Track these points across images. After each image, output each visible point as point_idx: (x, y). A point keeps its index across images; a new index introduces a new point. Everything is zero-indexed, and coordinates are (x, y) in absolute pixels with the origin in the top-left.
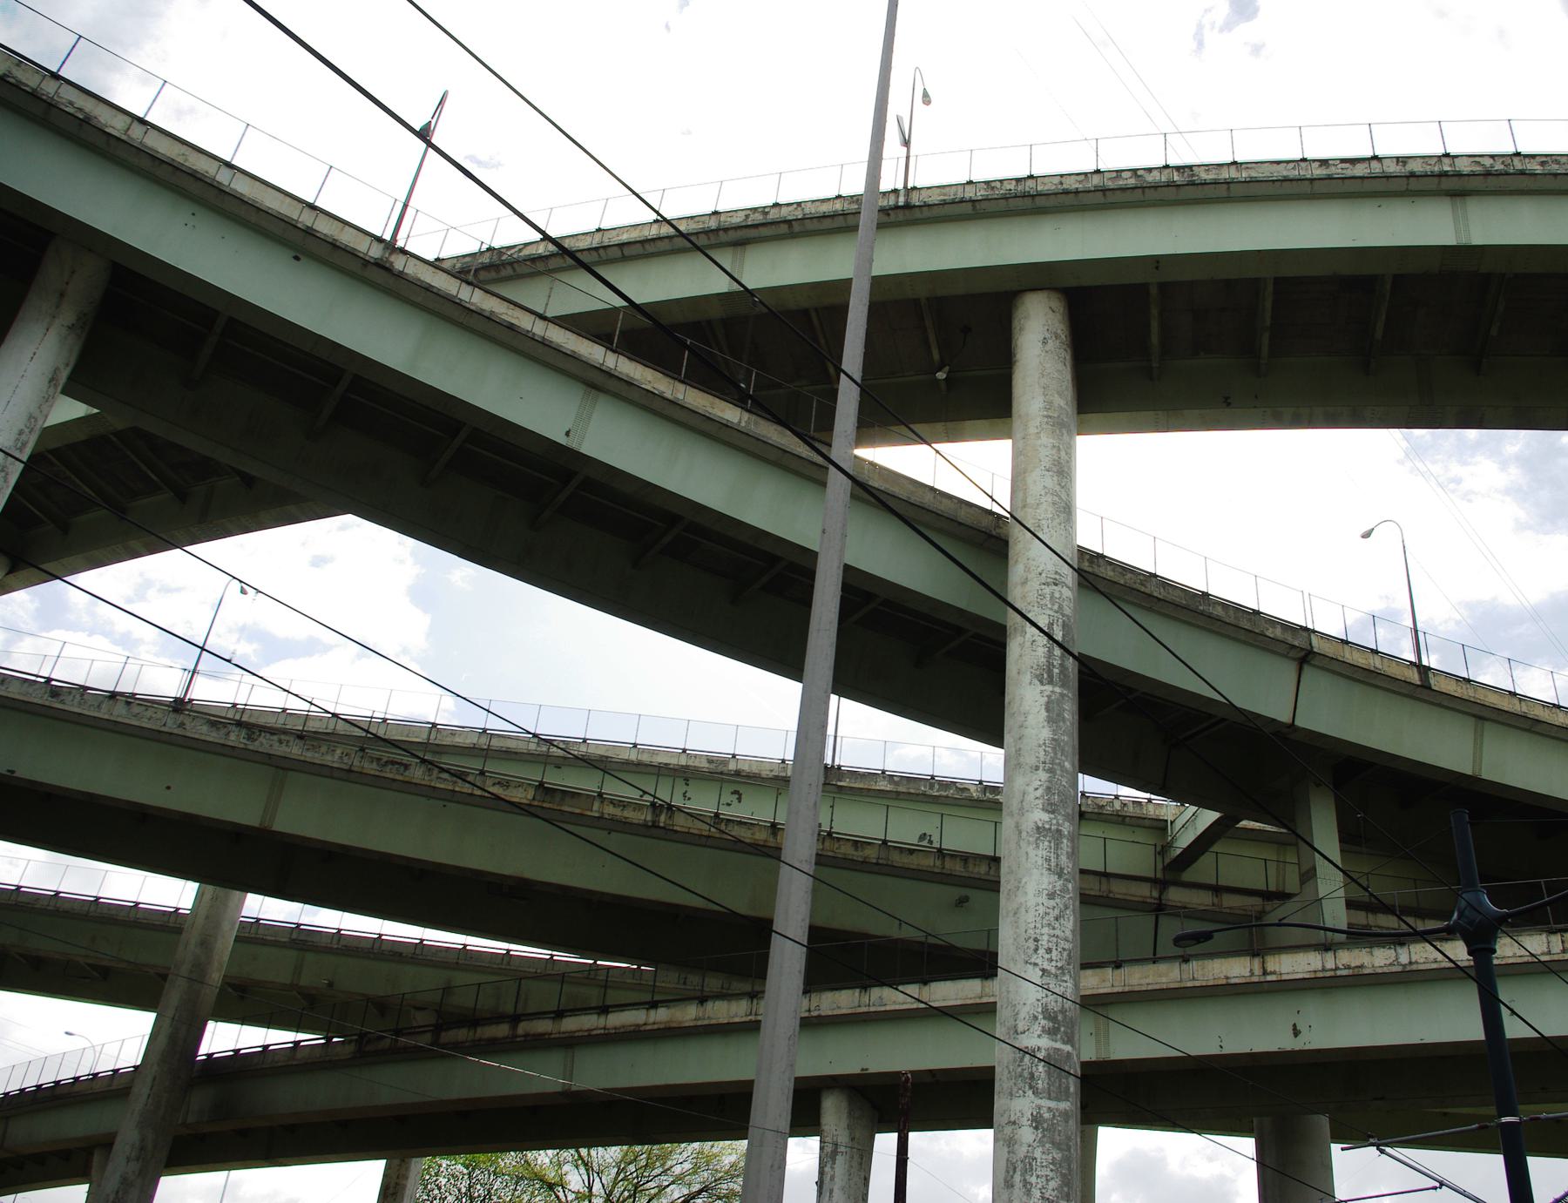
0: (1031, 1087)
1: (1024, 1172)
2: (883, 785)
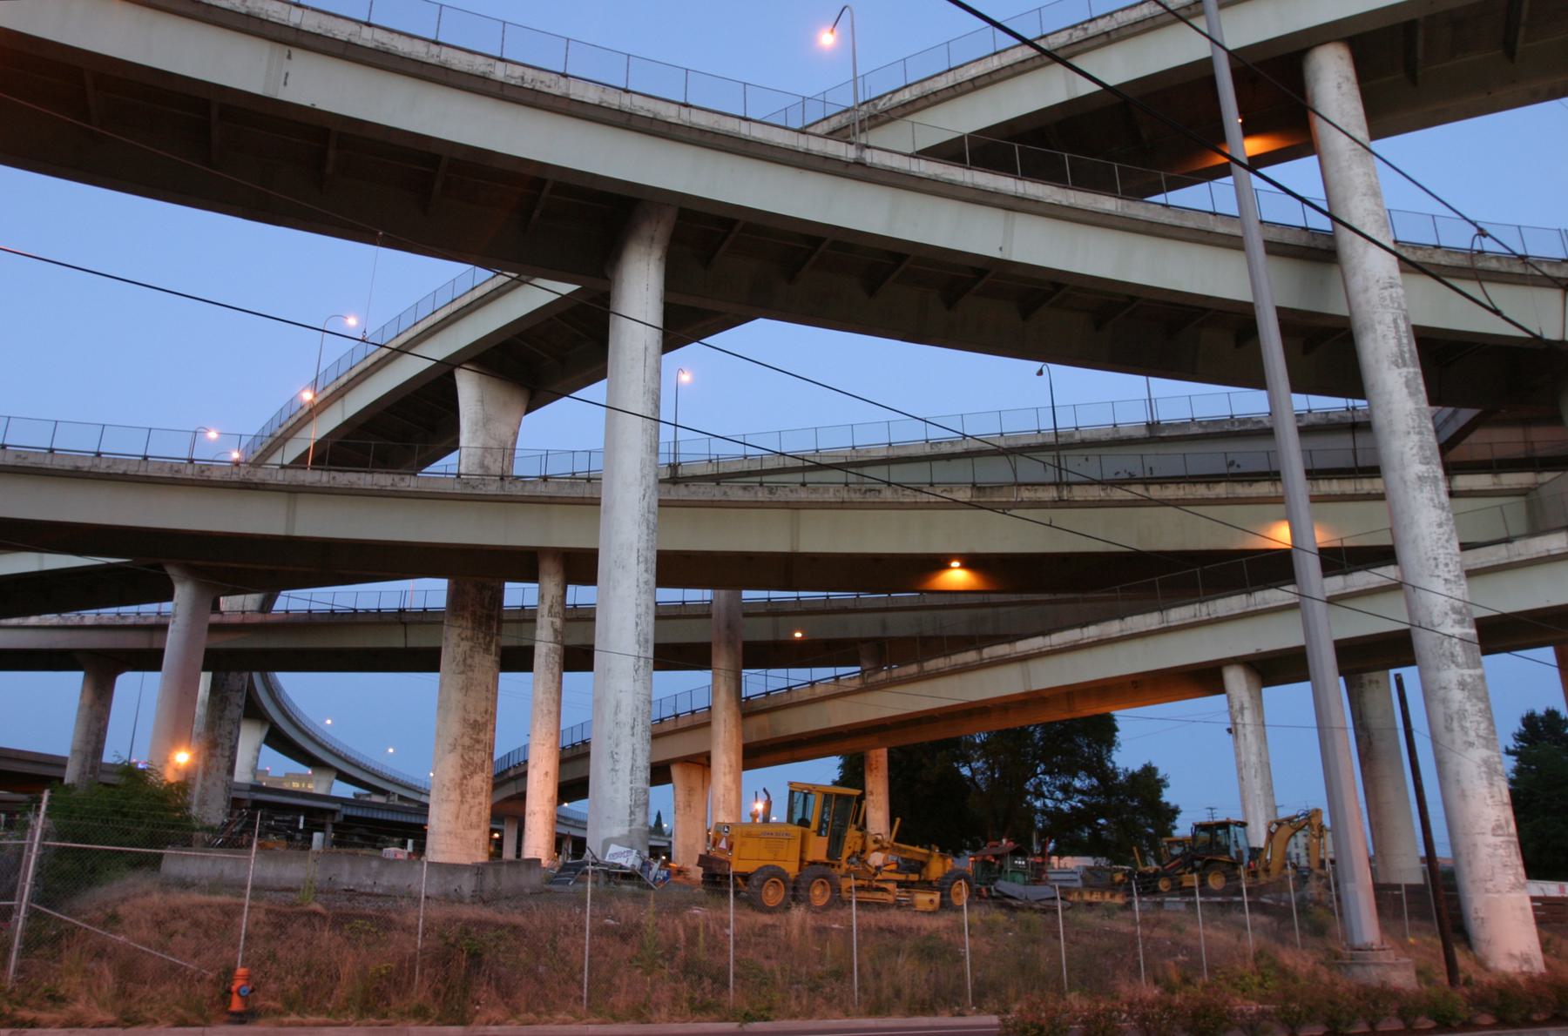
0: (1453, 662)
1: (1460, 720)
2: (1195, 430)
